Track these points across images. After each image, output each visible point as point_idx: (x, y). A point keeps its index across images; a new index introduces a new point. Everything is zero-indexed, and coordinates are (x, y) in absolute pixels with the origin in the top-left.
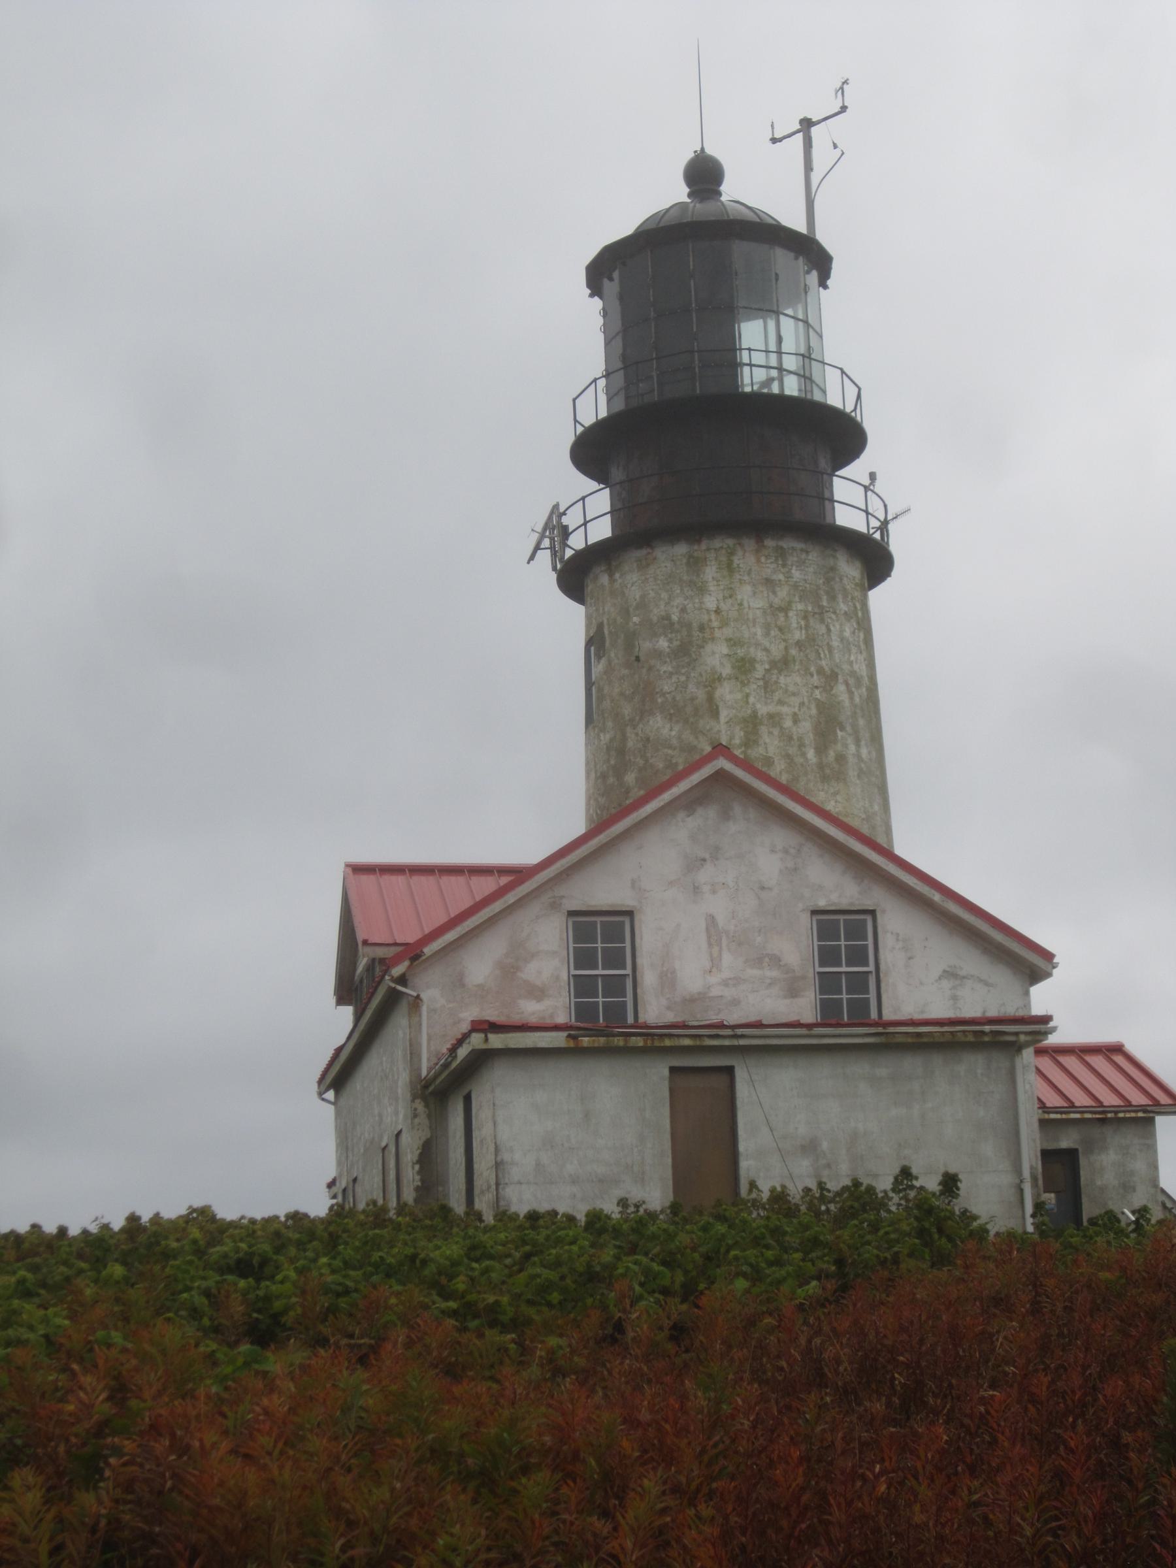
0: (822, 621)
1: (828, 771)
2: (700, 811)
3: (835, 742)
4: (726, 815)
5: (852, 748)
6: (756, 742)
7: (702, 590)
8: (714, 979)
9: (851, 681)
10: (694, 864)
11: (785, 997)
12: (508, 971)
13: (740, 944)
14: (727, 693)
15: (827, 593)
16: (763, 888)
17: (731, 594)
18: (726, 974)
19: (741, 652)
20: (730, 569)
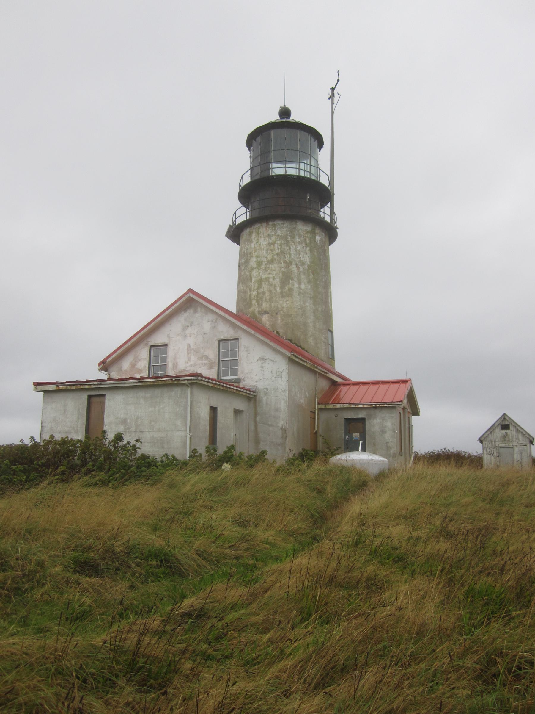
0: (287, 245)
1: (284, 294)
2: (188, 311)
3: (289, 284)
4: (195, 311)
5: (296, 285)
6: (261, 287)
7: (251, 242)
8: (188, 365)
9: (299, 264)
10: (185, 328)
11: (208, 369)
12: (133, 365)
13: (197, 353)
14: (255, 273)
15: (291, 236)
16: (205, 334)
17: (258, 241)
18: (192, 363)
19: (259, 259)
20: (258, 234)
